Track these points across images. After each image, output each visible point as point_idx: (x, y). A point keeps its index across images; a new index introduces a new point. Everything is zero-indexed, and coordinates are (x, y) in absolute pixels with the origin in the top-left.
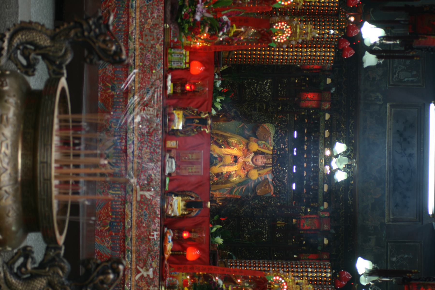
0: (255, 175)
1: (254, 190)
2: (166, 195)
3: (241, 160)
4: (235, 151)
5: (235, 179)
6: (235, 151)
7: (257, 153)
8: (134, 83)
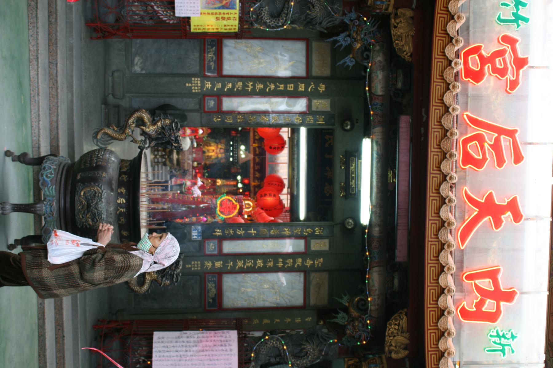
0: (220, 156)
1: (220, 161)
2: (193, 161)
3: (215, 151)
4: (213, 148)
5: (213, 157)
6: (213, 148)
7: (221, 148)
8: (29, 59)
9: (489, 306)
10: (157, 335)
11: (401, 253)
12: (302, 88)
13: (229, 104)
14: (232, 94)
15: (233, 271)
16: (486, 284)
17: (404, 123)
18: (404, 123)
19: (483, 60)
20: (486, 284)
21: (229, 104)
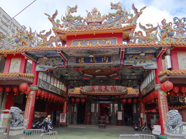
9: (114, 88)
10: (118, 119)
11: (109, 96)
12: (96, 102)
13: (97, 112)
14: (96, 111)
15: (114, 111)
16: (112, 88)
17: (98, 96)
18: (98, 96)
19: (93, 89)
20: (112, 88)
21: (97, 112)
